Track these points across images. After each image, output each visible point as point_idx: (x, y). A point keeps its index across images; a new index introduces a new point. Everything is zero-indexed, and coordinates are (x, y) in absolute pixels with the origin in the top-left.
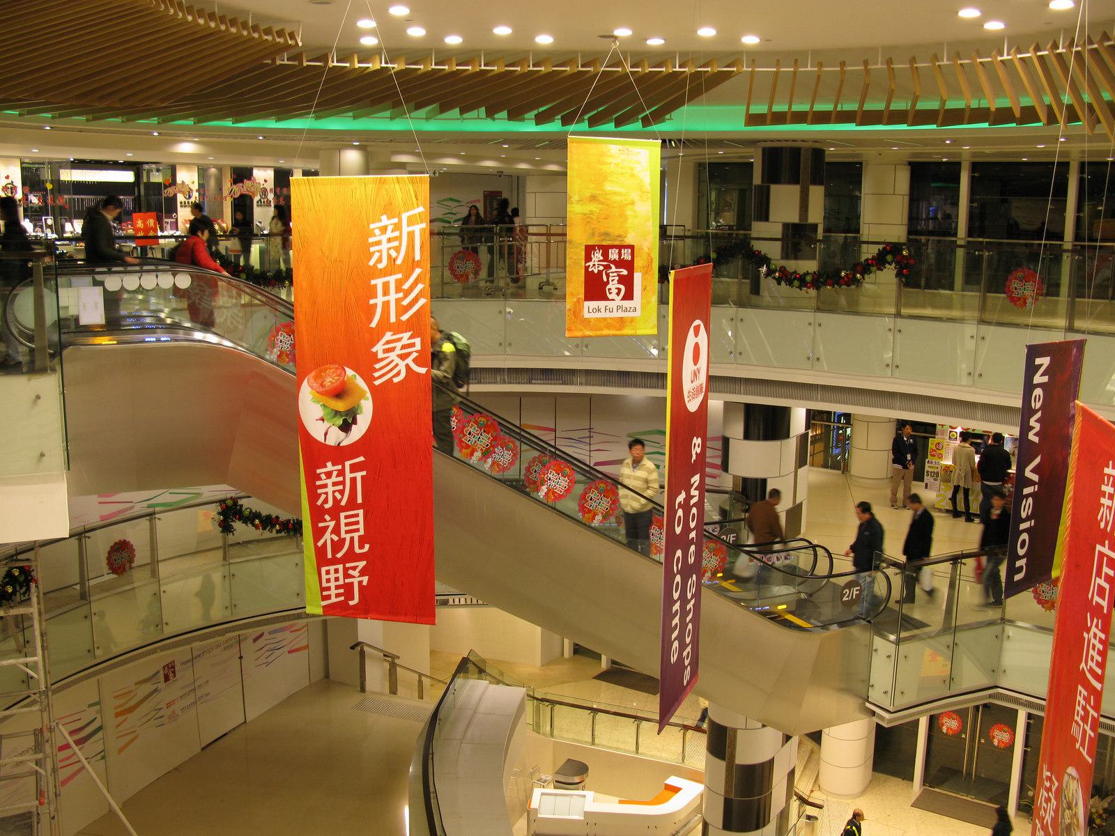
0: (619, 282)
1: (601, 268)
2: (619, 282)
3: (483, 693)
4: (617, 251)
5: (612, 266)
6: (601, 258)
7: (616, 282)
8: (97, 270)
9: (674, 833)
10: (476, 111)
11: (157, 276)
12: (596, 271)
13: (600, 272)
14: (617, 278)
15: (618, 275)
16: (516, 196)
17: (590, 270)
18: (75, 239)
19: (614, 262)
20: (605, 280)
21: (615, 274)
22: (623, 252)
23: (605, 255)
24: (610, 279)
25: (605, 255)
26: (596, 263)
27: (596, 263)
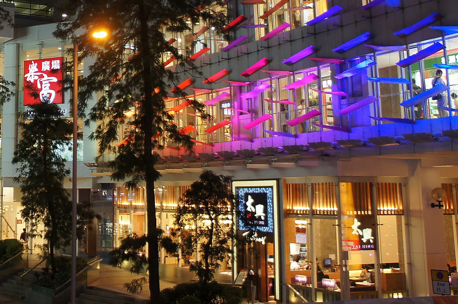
0: (51, 88)
1: (36, 78)
2: (51, 88)
3: (239, 123)
4: (48, 62)
5: (44, 75)
6: (37, 70)
7: (47, 88)
8: (163, 262)
9: (23, 231)
10: (418, 62)
11: (248, 57)
12: (32, 81)
13: (36, 81)
14: (49, 85)
15: (50, 83)
16: (256, 9)
17: (28, 80)
18: (125, 210)
19: (46, 72)
20: (39, 87)
21: (47, 82)
22: (53, 63)
23: (39, 67)
24: (43, 86)
25: (39, 67)
26: (33, 74)
27: (33, 74)
